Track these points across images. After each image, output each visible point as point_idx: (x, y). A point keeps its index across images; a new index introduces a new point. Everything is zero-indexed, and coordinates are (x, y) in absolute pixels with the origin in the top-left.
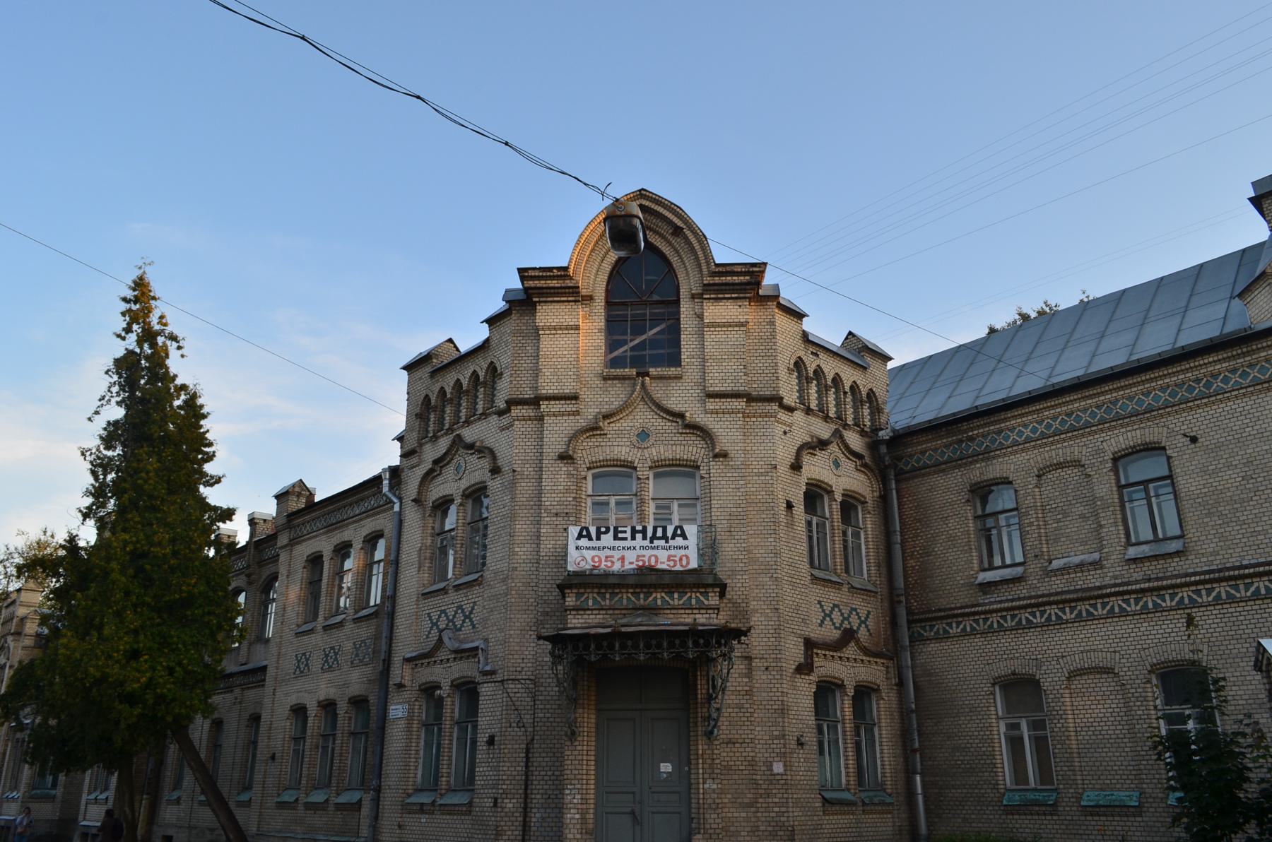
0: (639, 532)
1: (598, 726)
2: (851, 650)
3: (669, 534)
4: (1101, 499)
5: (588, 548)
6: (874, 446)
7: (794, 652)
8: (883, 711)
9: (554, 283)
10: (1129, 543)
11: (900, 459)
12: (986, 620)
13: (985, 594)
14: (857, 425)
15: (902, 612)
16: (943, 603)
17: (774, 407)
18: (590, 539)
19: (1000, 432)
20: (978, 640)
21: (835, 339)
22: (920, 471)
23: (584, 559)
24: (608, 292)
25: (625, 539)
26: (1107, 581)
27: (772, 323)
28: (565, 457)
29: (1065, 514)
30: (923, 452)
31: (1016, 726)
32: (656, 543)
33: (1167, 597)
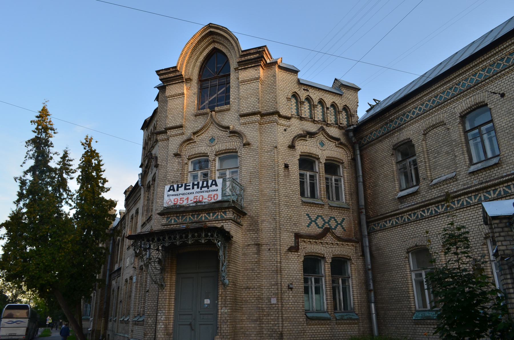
0: (196, 185)
1: (177, 281)
2: (329, 238)
3: (209, 185)
4: (455, 140)
5: (173, 195)
6: (346, 134)
7: (290, 241)
8: (354, 271)
9: (171, 75)
10: (471, 163)
11: (362, 138)
12: (402, 217)
13: (401, 203)
14: (337, 124)
15: (363, 218)
16: (383, 211)
17: (276, 117)
18: (174, 191)
19: (404, 114)
20: (399, 229)
21: (328, 84)
22: (371, 143)
23: (170, 200)
24: (200, 75)
25: (189, 189)
26: (460, 187)
27: (274, 76)
28: (177, 155)
29: (438, 153)
30: (371, 133)
31: (421, 275)
32: (203, 189)
33: (492, 192)
